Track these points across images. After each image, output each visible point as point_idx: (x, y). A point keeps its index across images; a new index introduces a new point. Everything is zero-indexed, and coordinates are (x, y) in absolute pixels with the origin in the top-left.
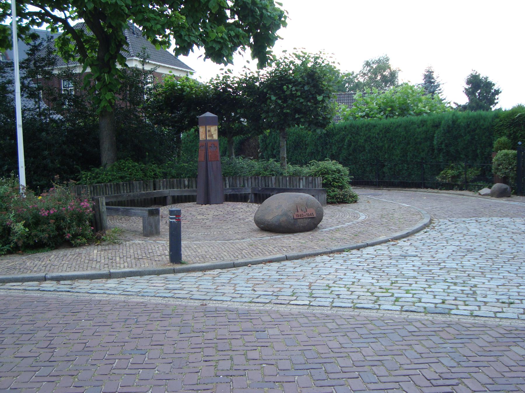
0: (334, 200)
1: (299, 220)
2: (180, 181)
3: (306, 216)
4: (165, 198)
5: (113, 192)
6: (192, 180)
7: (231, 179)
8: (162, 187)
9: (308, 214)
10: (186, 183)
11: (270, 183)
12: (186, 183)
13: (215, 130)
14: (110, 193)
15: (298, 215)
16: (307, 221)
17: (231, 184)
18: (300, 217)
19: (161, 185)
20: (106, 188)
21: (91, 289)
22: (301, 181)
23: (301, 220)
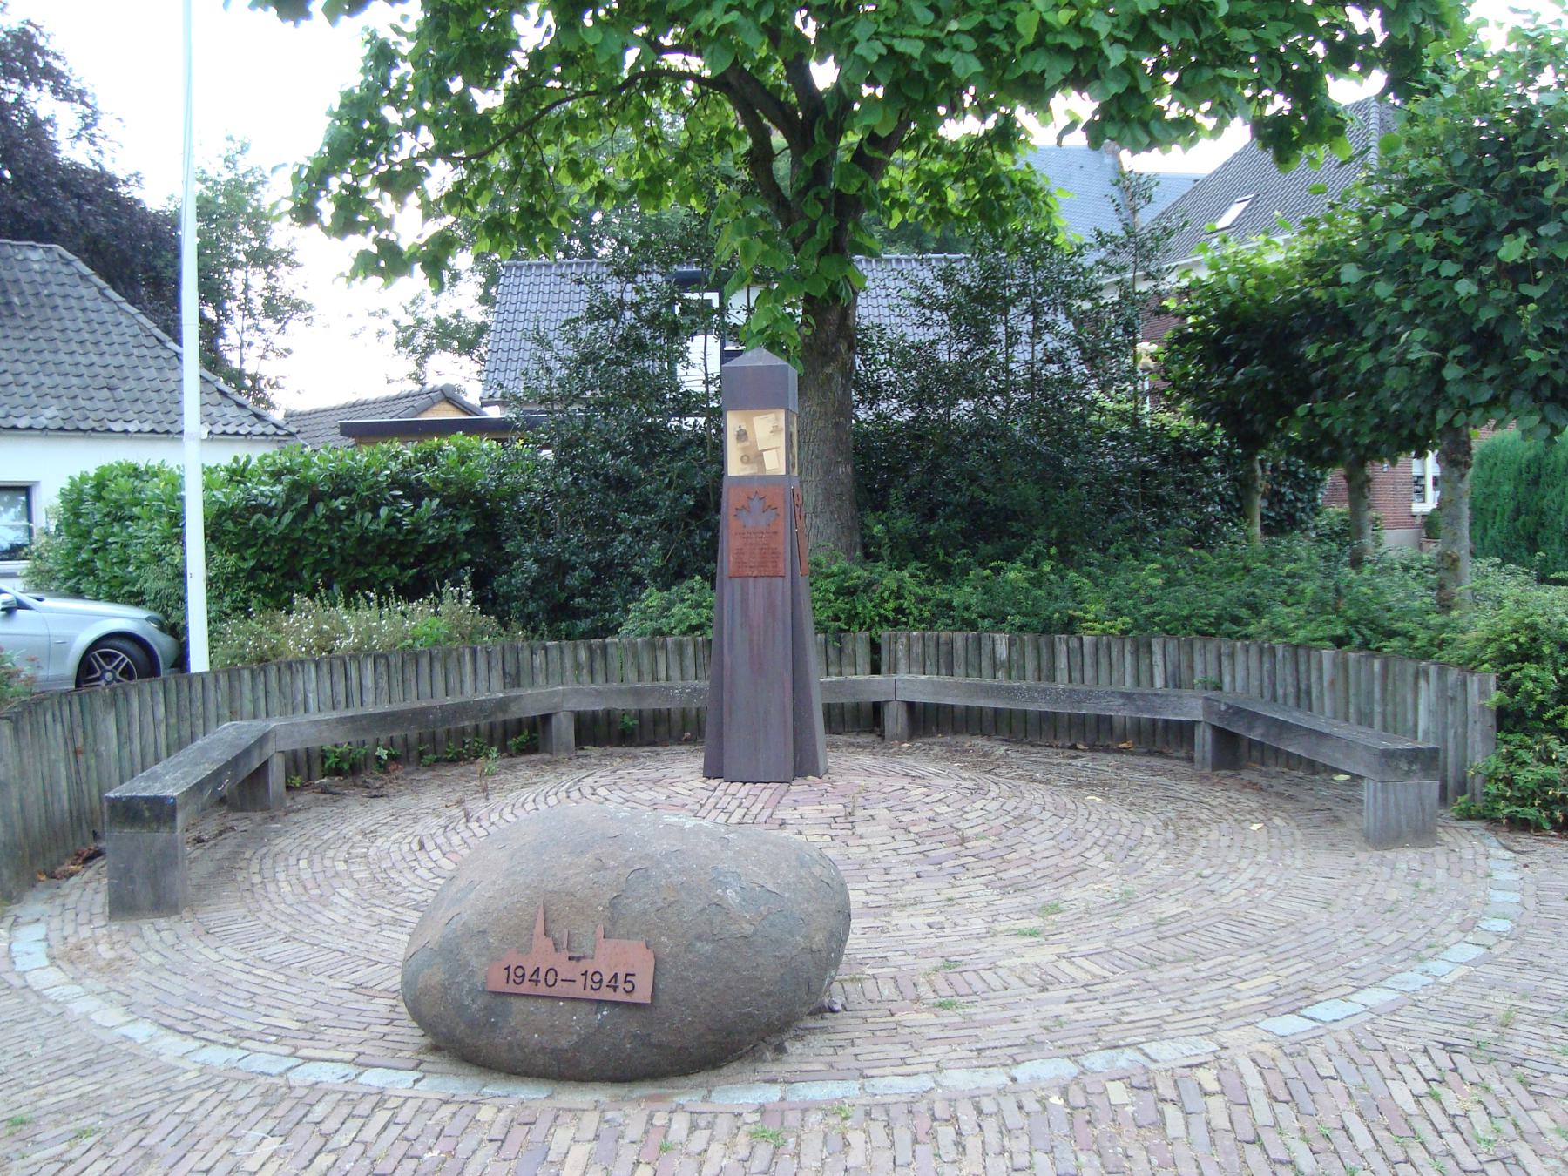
0: (1531, 813)
1: (517, 1004)
2: (979, 640)
3: (577, 990)
4: (877, 708)
5: (692, 672)
6: (1023, 642)
7: (1172, 645)
8: (902, 663)
9: (593, 979)
10: (1002, 651)
11: (1314, 678)
12: (1002, 651)
13: (775, 430)
14: (675, 673)
15: (516, 974)
16: (579, 1022)
17: (1170, 668)
18: (526, 987)
19: (900, 654)
20: (654, 660)
21: (1142, 969)
22: (1422, 683)
23: (531, 1005)
